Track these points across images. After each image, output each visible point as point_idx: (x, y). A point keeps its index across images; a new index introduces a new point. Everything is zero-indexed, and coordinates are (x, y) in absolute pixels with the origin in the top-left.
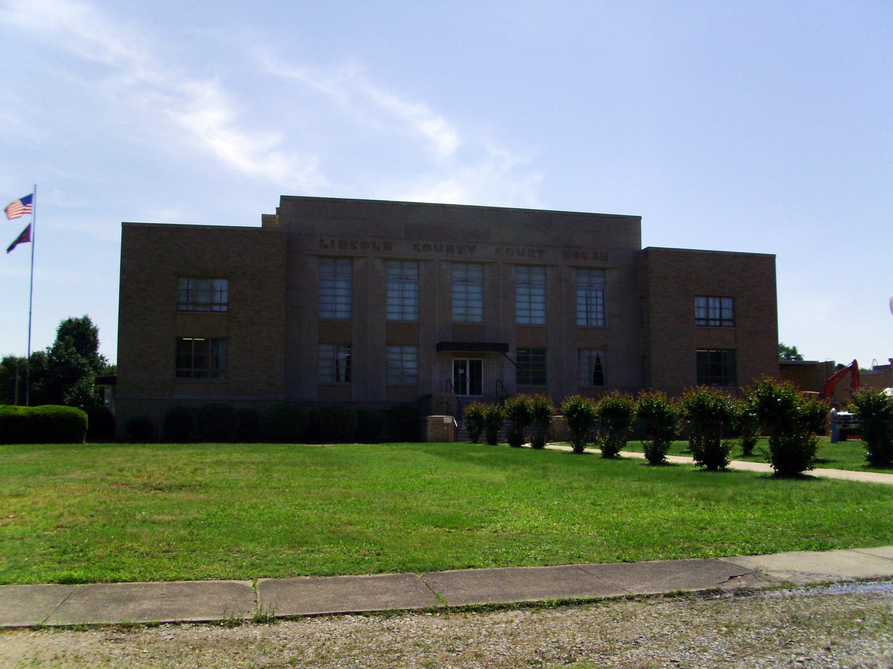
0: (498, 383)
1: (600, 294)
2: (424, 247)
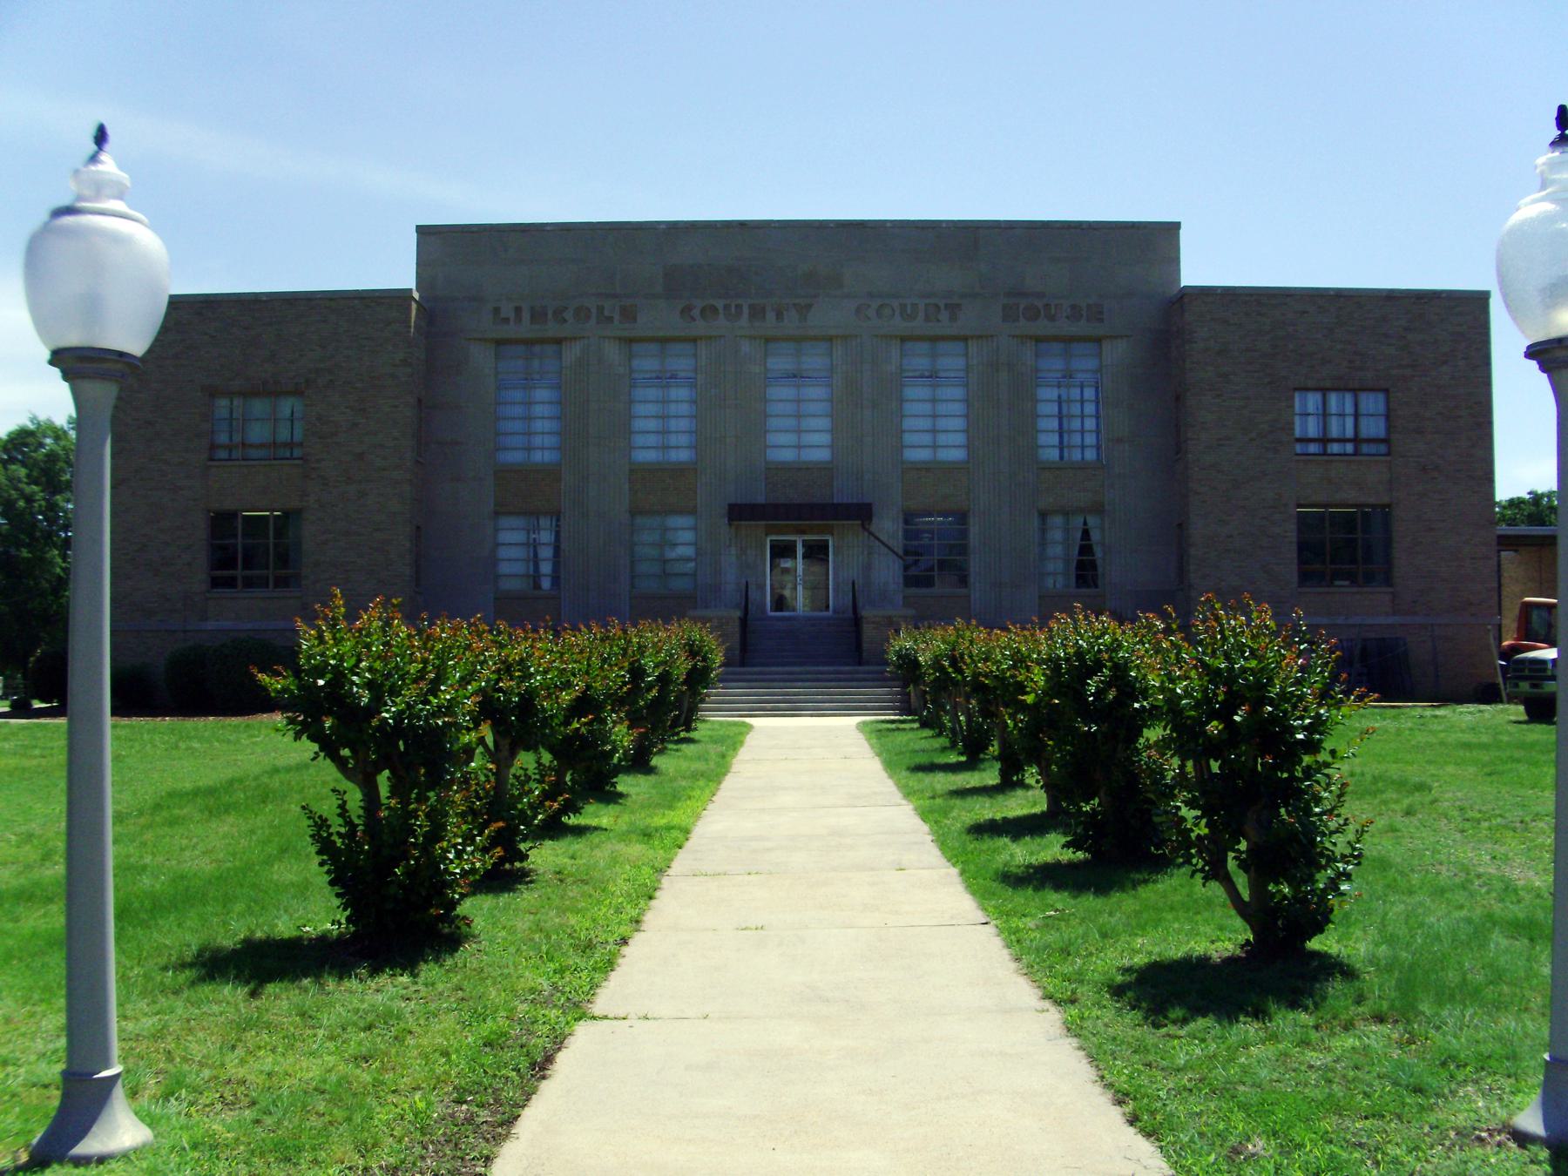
2: (703, 311)
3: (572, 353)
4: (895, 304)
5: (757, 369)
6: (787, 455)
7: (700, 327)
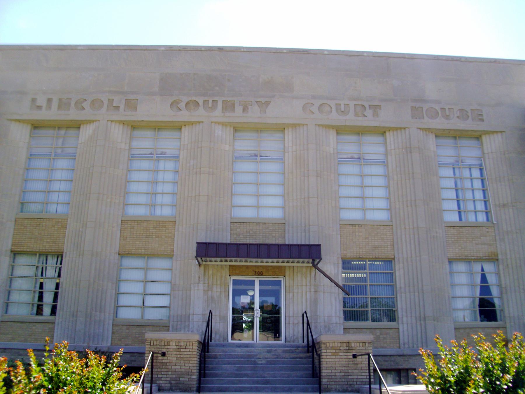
0: (305, 315)
1: (476, 173)
2: (187, 104)
3: (86, 132)
4: (333, 103)
5: (227, 148)
6: (248, 214)
7: (184, 116)
